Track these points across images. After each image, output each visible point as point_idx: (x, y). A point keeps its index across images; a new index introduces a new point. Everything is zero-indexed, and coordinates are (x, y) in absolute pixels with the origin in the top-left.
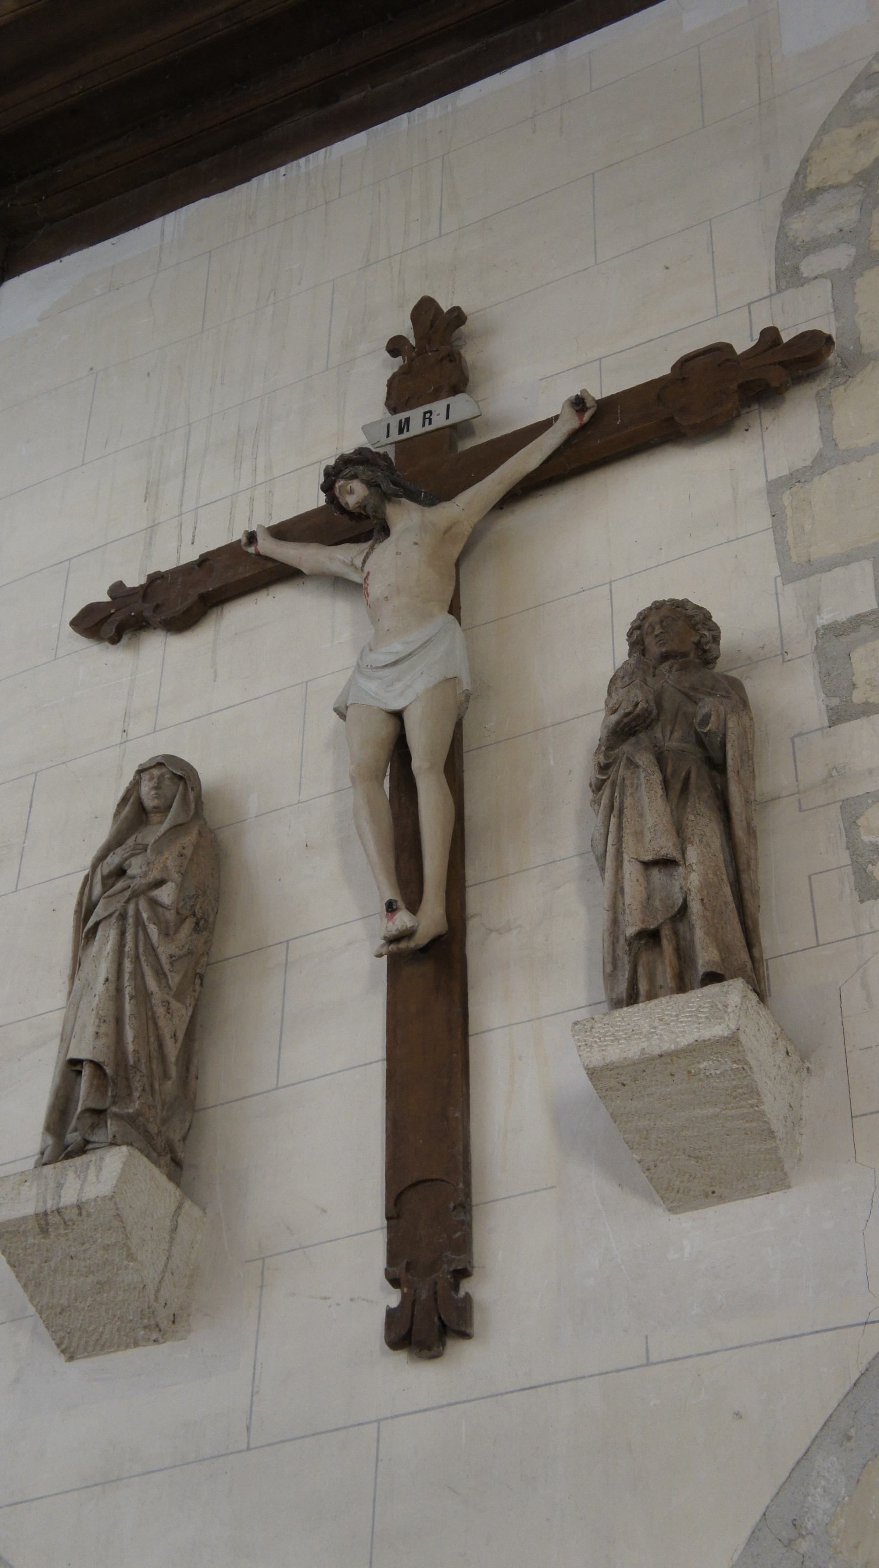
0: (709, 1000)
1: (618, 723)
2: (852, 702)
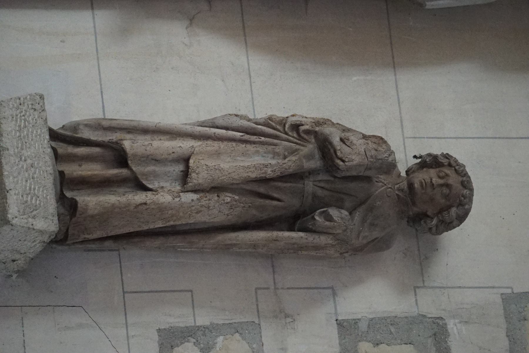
0: (42, 204)
1: (331, 144)
2: (360, 341)
